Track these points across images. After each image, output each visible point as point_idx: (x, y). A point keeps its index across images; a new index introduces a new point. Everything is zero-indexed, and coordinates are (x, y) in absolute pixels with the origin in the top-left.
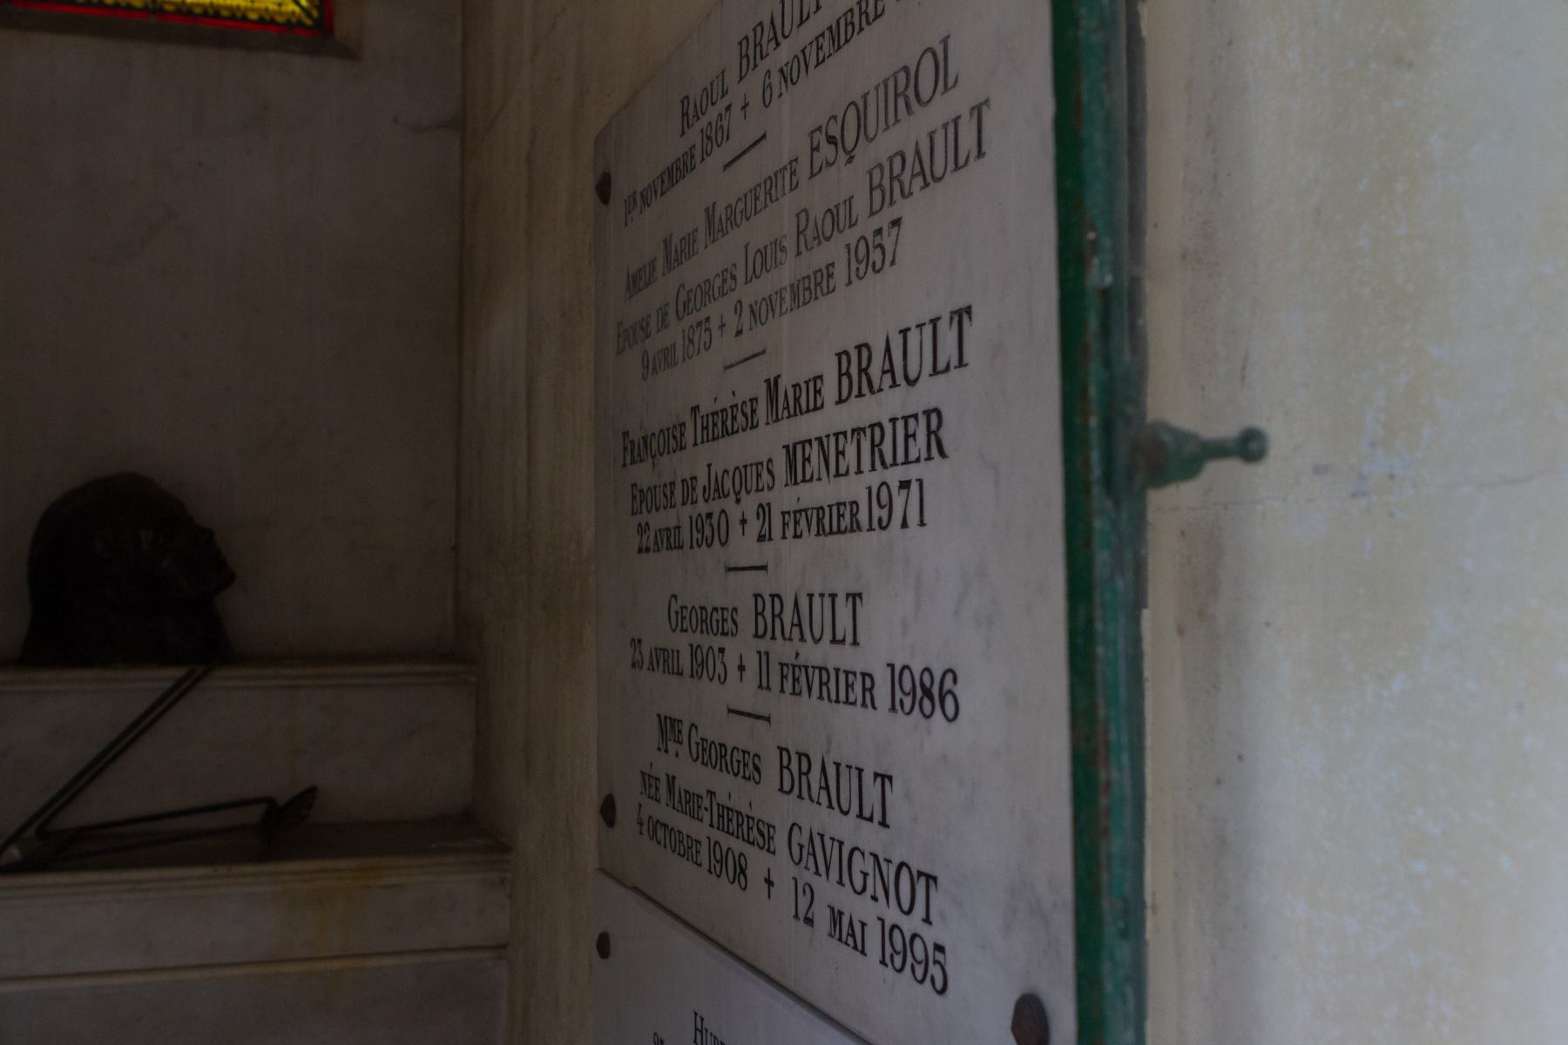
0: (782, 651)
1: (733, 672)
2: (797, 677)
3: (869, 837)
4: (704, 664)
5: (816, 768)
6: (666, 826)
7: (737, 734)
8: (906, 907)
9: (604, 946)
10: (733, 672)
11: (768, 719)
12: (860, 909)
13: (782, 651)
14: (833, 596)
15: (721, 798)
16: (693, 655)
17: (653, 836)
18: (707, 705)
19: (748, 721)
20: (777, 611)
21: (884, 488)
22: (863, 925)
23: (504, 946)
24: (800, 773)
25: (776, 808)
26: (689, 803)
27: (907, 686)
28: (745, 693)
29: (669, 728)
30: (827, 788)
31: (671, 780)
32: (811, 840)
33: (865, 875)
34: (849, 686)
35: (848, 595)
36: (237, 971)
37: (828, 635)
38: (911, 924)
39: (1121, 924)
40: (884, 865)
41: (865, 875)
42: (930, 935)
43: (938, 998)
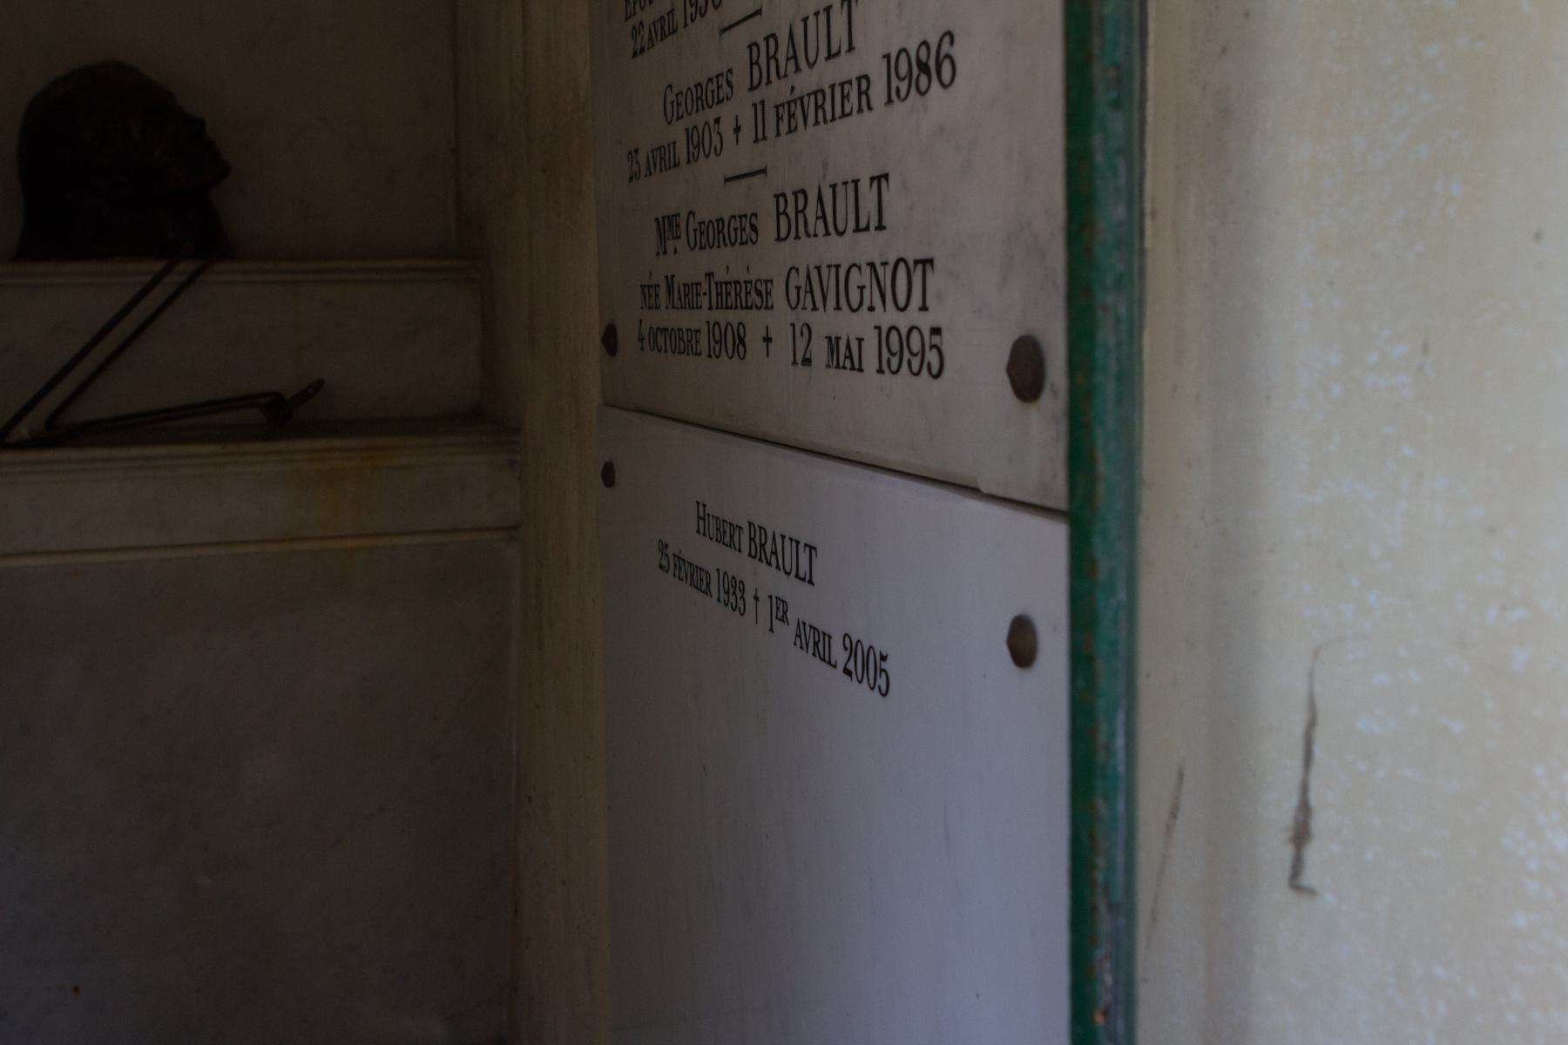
0: (777, 92)
1: (729, 136)
2: (792, 114)
3: (867, 247)
4: (700, 144)
5: (813, 198)
6: (666, 329)
7: (732, 202)
8: (902, 303)
9: (608, 475)
10: (729, 136)
11: (764, 171)
12: (857, 326)
13: (777, 92)
14: (856, 182)
15: (721, 276)
16: (689, 138)
17: (655, 346)
18: (703, 189)
19: (744, 181)
20: (800, 207)
21: (903, 55)
22: (860, 340)
23: (515, 528)
24: (797, 212)
25: (771, 259)
26: (687, 296)
27: (903, 70)
28: (740, 156)
29: (667, 227)
30: (824, 217)
31: (670, 280)
32: (808, 277)
33: (862, 288)
34: (845, 97)
35: (872, 179)
36: (251, 549)
37: (852, 225)
38: (913, 316)
39: (1113, 95)
40: (880, 270)
41: (862, 288)
42: (925, 321)
43: (935, 382)
